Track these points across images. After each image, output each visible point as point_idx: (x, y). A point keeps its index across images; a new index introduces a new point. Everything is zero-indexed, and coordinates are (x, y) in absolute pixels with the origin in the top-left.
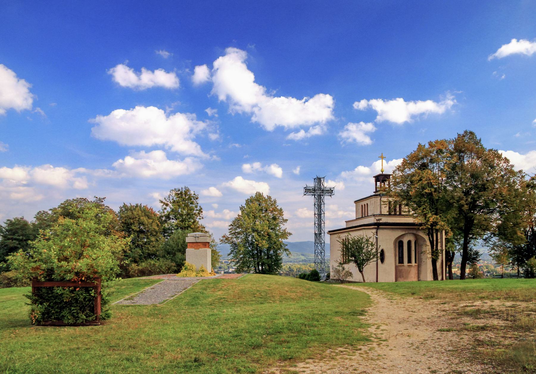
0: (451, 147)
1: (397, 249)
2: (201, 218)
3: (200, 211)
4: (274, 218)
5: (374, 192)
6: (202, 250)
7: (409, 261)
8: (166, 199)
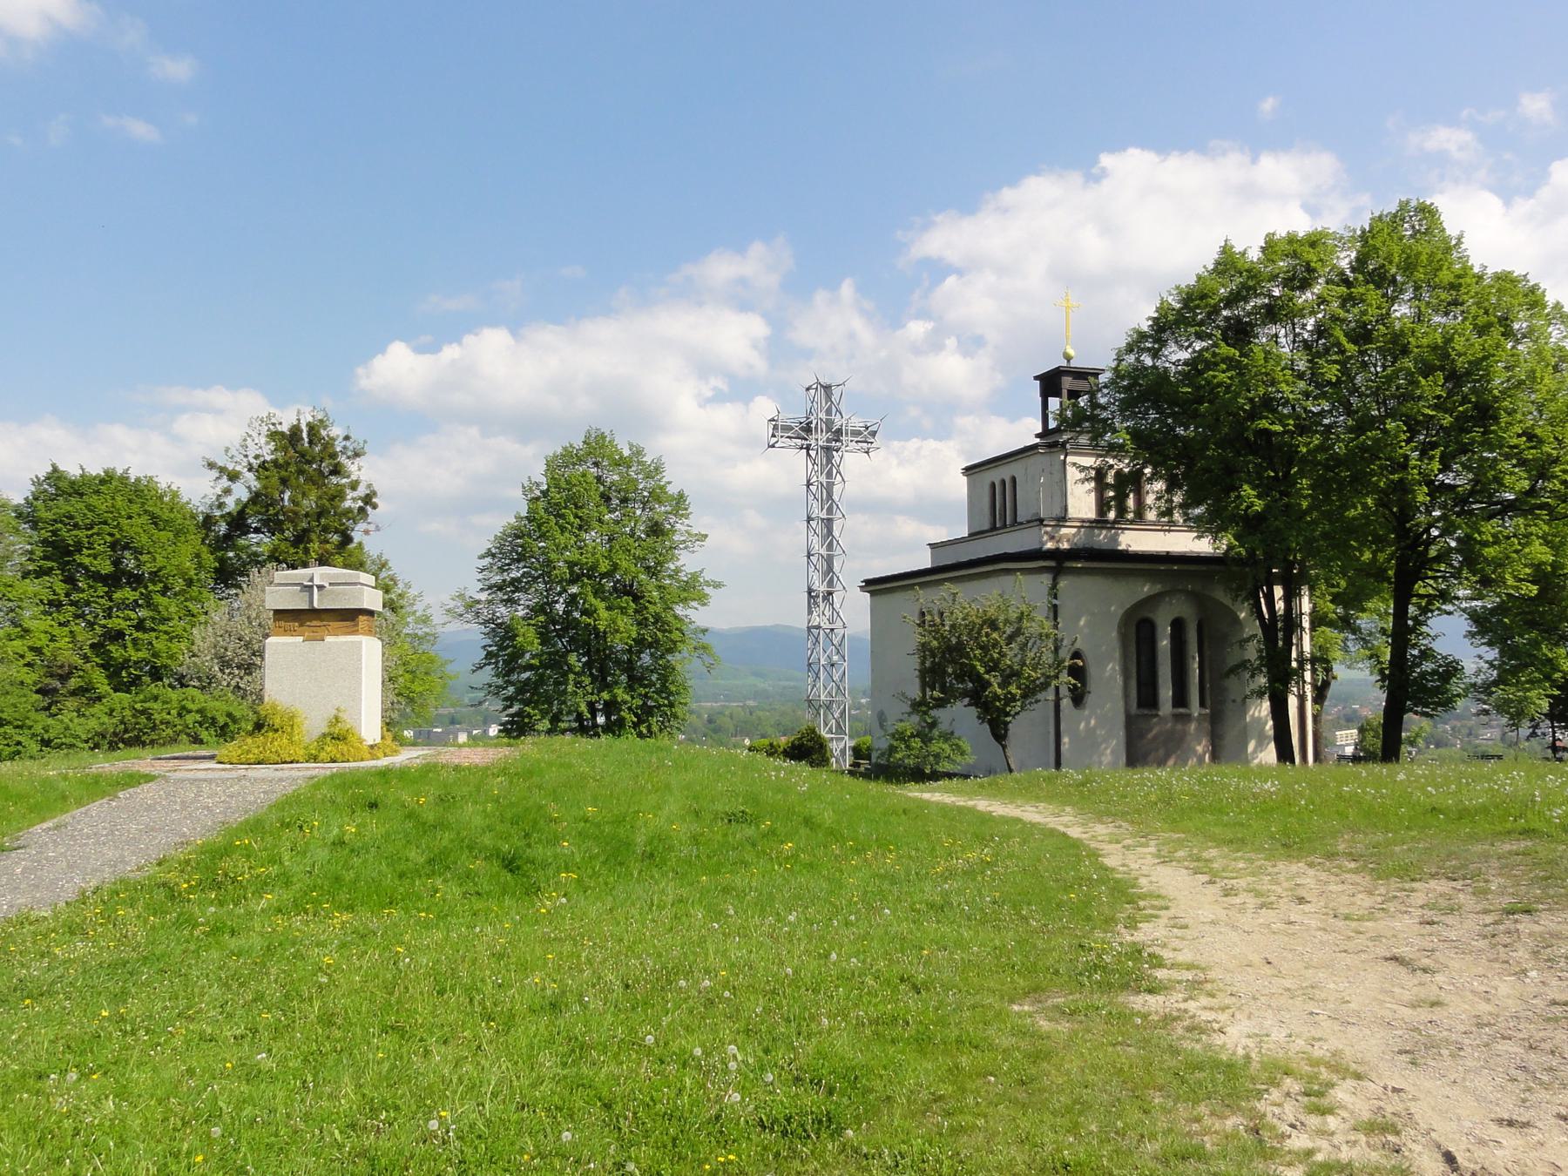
0: (1345, 260)
1: (1133, 649)
2: (371, 527)
3: (366, 503)
4: (656, 530)
5: (1038, 436)
6: (337, 641)
7: (1180, 699)
8: (233, 452)
